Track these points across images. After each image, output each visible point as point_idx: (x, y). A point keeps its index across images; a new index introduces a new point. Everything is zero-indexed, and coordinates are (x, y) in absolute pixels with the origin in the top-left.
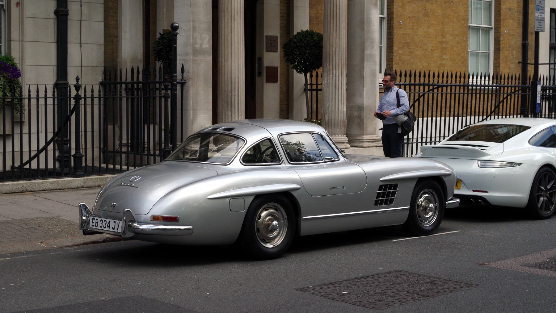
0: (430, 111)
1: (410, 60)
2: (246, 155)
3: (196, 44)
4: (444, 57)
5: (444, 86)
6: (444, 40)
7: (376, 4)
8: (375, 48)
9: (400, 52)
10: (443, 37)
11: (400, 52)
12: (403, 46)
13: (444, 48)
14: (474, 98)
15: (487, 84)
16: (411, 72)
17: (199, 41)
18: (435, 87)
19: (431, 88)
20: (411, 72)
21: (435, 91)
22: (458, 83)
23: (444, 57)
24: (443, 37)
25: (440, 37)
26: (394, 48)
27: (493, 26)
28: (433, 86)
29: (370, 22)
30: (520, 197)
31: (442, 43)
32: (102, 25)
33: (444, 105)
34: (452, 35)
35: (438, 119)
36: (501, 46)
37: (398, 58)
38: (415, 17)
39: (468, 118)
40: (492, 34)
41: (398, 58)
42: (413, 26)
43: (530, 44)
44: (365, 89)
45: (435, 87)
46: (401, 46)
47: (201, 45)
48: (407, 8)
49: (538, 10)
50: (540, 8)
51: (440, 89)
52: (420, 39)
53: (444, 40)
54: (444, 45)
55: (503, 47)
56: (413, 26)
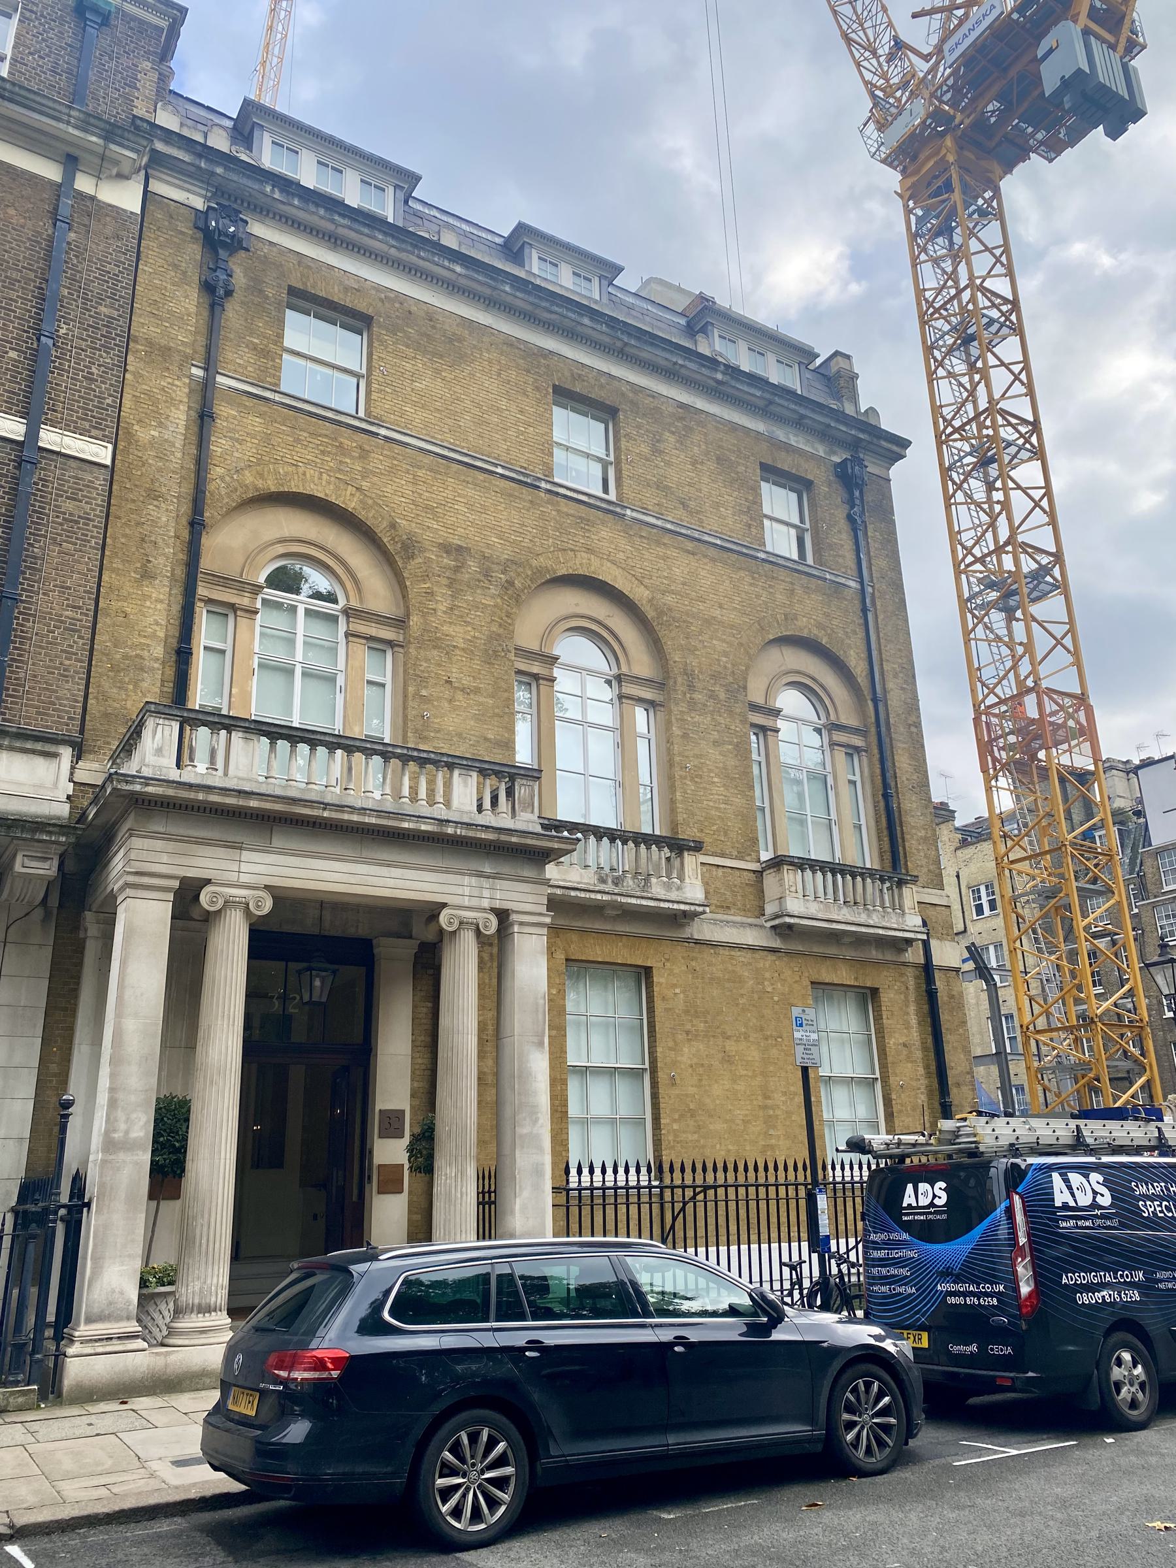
0: (754, 1231)
1: (698, 1141)
2: (363, 1321)
3: (115, 1131)
4: (771, 1132)
5: (710, 1187)
6: (769, 1102)
7: (541, 1044)
8: (541, 1121)
9: (675, 1126)
10: (766, 1097)
11: (675, 1126)
12: (682, 1116)
13: (770, 1116)
14: (743, 1212)
15: (632, 1183)
16: (795, 1163)
17: (123, 1126)
18: (698, 1190)
19: (689, 1193)
20: (795, 1163)
21: (701, 1197)
22: (678, 1182)
23: (771, 1132)
24: (766, 1097)
25: (760, 1098)
26: (662, 1121)
27: (878, 1075)
28: (694, 1187)
29: (525, 1076)
30: (797, 1442)
31: (765, 1107)
32: (30, 1105)
33: (783, 1219)
34: (784, 1094)
35: (734, 1248)
36: (895, 1110)
37: (671, 1138)
38: (702, 1065)
39: (723, 1249)
40: (878, 1086)
41: (671, 1138)
42: (700, 1080)
43: (955, 1102)
44: (518, 1200)
45: (698, 1190)
46: (676, 1117)
47: (127, 1132)
48: (686, 1050)
49: (801, 1025)
50: (805, 1022)
51: (711, 1192)
52: (718, 1102)
53: (769, 1102)
54: (771, 1112)
55: (900, 1111)
56: (700, 1080)
